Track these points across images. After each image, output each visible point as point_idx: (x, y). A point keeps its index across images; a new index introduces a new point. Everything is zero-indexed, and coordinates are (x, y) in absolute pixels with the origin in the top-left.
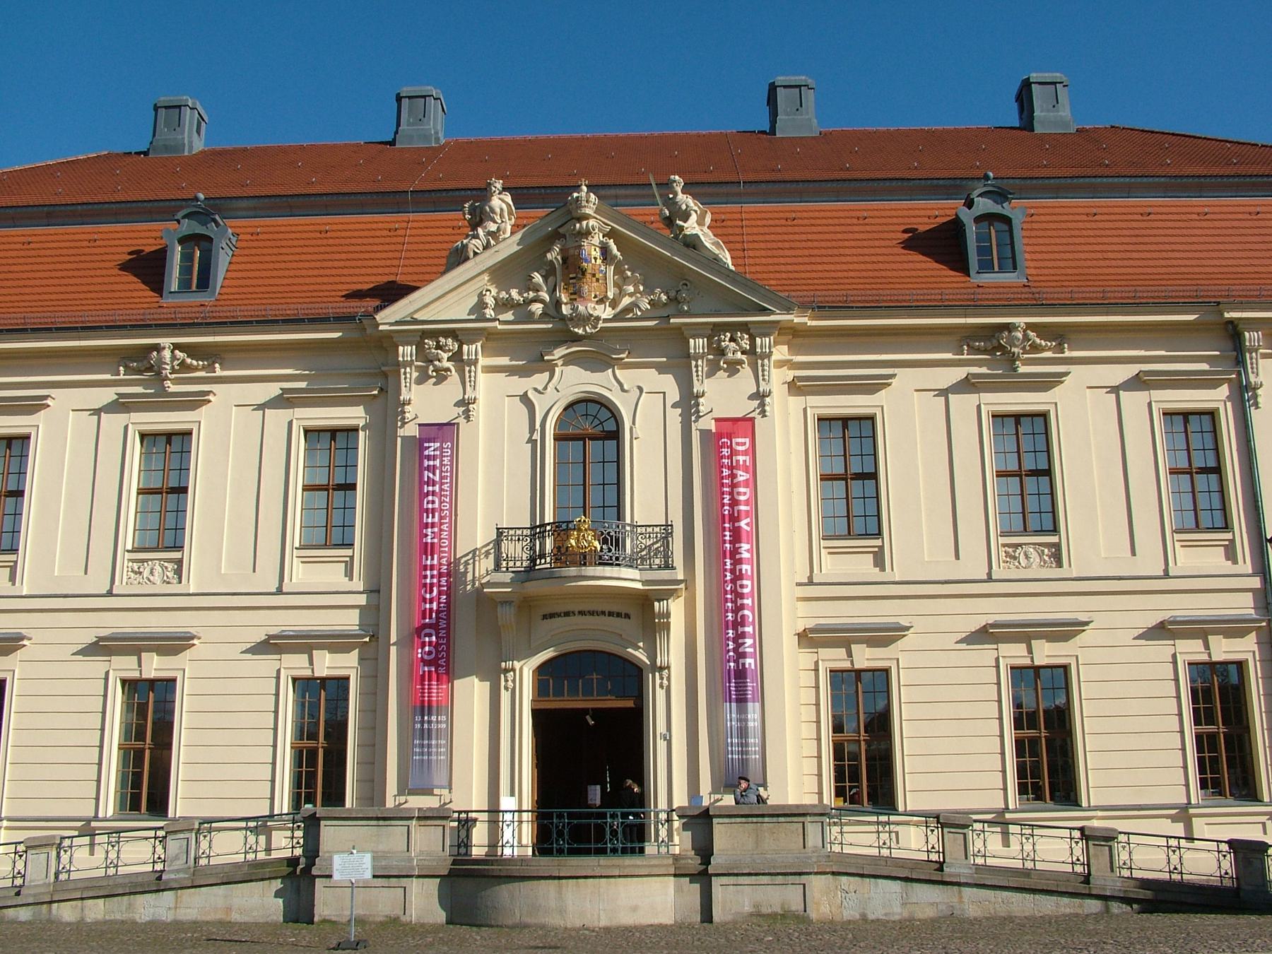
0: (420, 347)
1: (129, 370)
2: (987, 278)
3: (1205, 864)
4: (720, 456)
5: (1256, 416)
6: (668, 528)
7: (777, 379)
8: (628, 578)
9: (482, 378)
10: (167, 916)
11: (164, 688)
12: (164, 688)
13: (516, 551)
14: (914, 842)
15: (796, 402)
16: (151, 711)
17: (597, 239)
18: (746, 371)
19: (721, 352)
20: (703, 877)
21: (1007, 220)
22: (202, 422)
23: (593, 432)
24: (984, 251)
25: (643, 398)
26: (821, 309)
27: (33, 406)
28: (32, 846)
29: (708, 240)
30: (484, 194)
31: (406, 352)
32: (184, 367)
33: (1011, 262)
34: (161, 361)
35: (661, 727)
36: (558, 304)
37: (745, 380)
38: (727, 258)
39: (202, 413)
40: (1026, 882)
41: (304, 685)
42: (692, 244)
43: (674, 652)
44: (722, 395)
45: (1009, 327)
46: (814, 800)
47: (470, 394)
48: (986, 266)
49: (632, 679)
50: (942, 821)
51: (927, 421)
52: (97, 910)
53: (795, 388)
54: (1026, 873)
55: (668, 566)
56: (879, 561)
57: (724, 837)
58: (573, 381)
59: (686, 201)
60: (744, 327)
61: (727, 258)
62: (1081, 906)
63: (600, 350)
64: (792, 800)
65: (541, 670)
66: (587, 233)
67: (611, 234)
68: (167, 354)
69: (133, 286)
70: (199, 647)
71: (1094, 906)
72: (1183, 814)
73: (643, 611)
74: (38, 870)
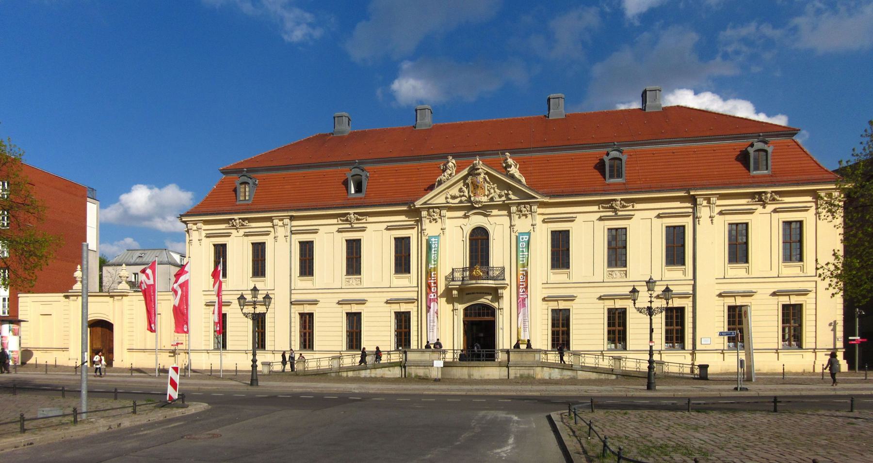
0: (428, 211)
1: (603, 207)
2: (612, 181)
4: (522, 244)
5: (698, 226)
6: (503, 269)
7: (539, 219)
8: (491, 283)
9: (447, 221)
10: (368, 376)
13: (458, 275)
17: (482, 175)
18: (529, 216)
19: (521, 211)
23: (479, 242)
24: (611, 171)
25: (498, 226)
27: (315, 232)
28: (333, 358)
29: (517, 174)
31: (424, 213)
32: (624, 206)
33: (619, 176)
34: (766, 198)
35: (501, 326)
36: (470, 197)
37: (529, 221)
38: (523, 180)
40: (595, 370)
41: (611, 312)
42: (512, 177)
44: (522, 224)
45: (615, 200)
46: (80, 298)
47: (534, 223)
48: (611, 176)
49: (491, 311)
51: (588, 231)
52: (350, 374)
54: (595, 368)
55: (504, 279)
56: (569, 277)
57: (513, 357)
58: (477, 220)
59: (510, 161)
60: (528, 203)
61: (523, 180)
62: (703, 390)
63: (485, 210)
65: (466, 310)
66: (479, 174)
67: (487, 173)
68: (769, 195)
70: (367, 304)
71: (614, 377)
73: (495, 293)
74: (335, 364)
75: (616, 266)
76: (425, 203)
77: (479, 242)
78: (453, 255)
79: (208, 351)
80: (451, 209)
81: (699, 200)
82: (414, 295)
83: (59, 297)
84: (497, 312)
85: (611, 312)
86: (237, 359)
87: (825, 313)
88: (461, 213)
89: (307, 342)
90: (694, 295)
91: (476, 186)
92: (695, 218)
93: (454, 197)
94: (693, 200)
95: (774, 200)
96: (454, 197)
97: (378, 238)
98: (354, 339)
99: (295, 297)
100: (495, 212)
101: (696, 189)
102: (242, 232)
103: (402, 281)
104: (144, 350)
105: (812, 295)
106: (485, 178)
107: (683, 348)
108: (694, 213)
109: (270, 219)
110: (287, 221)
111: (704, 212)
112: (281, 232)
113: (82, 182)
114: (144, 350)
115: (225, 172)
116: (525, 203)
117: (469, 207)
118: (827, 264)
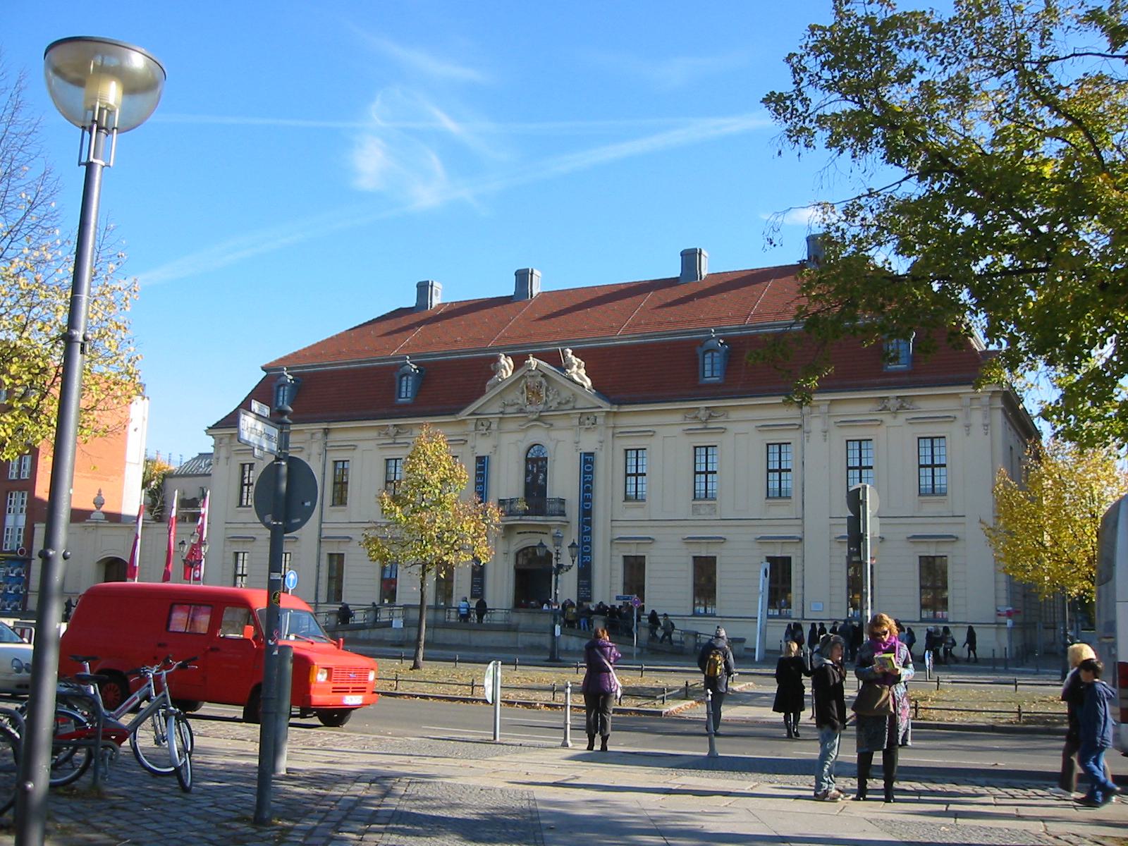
11: (787, 561)
12: (787, 561)
41: (697, 560)
58: (537, 435)
76: (473, 414)
85: (697, 560)
102: (902, 417)
106: (541, 383)
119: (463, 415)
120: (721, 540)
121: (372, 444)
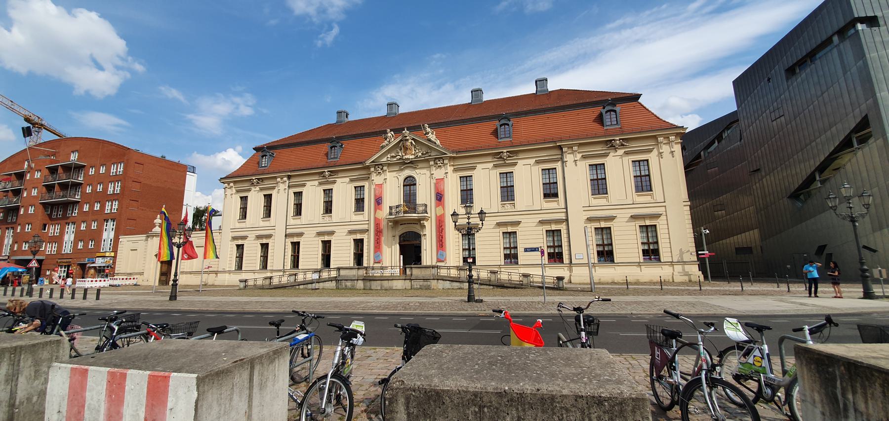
3: (550, 281)
14: (334, 274)
15: (455, 175)
16: (327, 245)
20: (470, 280)
21: (615, 111)
22: (304, 190)
23: (410, 183)
25: (424, 179)
26: (457, 152)
27: (304, 185)
30: (385, 132)
37: (443, 170)
38: (438, 142)
39: (475, 172)
42: (430, 140)
43: (427, 231)
44: (438, 173)
49: (418, 236)
50: (339, 269)
51: (486, 178)
53: (455, 170)
58: (407, 172)
59: (428, 130)
61: (438, 142)
63: (412, 164)
64: (429, 264)
67: (413, 139)
69: (597, 126)
72: (320, 271)
73: (418, 221)
75: (508, 200)
77: (410, 183)
78: (393, 195)
79: (230, 272)
80: (389, 165)
81: (565, 149)
82: (366, 227)
83: (143, 237)
84: (423, 238)
86: (253, 274)
87: (678, 234)
88: (397, 168)
89: (296, 263)
90: (567, 220)
91: (406, 149)
92: (563, 162)
93: (393, 157)
94: (560, 148)
95: (623, 145)
96: (393, 157)
97: (343, 190)
98: (326, 260)
99: (289, 231)
100: (420, 165)
101: (561, 141)
102: (258, 188)
103: (359, 217)
104: (191, 273)
105: (663, 218)
107: (562, 262)
108: (562, 159)
109: (655, 138)
110: (232, 184)
111: (569, 158)
112: (282, 187)
113: (183, 162)
114: (191, 273)
115: (257, 149)
116: (439, 159)
117: (404, 164)
118: (327, 155)
119: (368, 163)
120: (518, 223)
121: (316, 183)
